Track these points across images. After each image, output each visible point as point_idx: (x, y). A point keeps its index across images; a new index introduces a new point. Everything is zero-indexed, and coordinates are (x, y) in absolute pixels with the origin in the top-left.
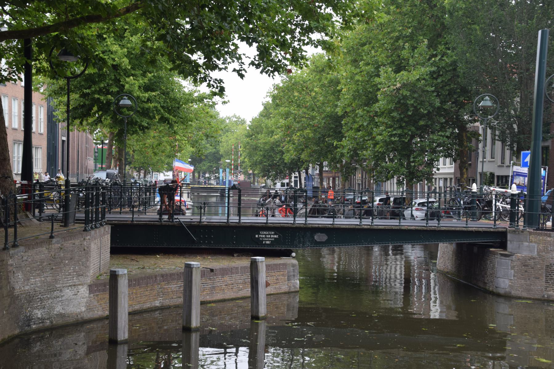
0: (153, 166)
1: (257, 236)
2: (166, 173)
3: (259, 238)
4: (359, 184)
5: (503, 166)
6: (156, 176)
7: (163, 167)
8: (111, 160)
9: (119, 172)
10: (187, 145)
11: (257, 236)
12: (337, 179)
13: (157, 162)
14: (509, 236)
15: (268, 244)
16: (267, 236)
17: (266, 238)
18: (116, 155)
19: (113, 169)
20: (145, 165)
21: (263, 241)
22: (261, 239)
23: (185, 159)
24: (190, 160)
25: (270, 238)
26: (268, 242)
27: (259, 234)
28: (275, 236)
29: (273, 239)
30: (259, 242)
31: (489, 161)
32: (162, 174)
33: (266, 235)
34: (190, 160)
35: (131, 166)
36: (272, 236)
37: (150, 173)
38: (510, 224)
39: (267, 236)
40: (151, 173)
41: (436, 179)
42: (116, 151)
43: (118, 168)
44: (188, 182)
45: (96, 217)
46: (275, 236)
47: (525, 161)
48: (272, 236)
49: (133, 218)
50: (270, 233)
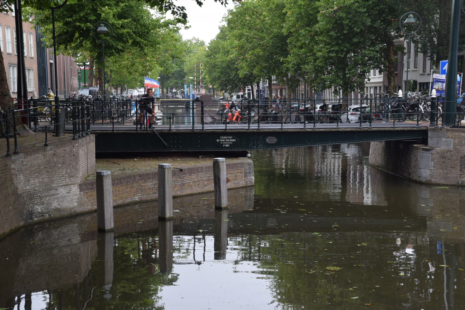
0: (128, 84)
1: (218, 141)
2: (139, 90)
3: (220, 142)
4: (302, 94)
5: (425, 74)
6: (131, 92)
7: (136, 84)
8: (93, 79)
9: (100, 90)
10: (156, 65)
11: (218, 141)
12: (284, 90)
13: (132, 80)
14: (430, 134)
15: (227, 147)
16: (227, 140)
17: (226, 142)
18: (96, 75)
19: (94, 87)
20: (121, 83)
21: (223, 144)
22: (221, 143)
23: (155, 77)
24: (159, 78)
25: (229, 142)
26: (227, 146)
27: (219, 139)
28: (233, 140)
29: (232, 143)
30: (220, 145)
31: (413, 71)
32: (136, 91)
33: (225, 139)
34: (159, 78)
35: (110, 84)
36: (231, 140)
37: (125, 89)
38: (431, 124)
39: (227, 140)
40: (127, 90)
41: (367, 88)
42: (96, 72)
43: (98, 86)
44: (158, 97)
45: (82, 128)
46: (233, 140)
47: (444, 69)
48: (231, 140)
49: (113, 128)
50: (229, 137)
